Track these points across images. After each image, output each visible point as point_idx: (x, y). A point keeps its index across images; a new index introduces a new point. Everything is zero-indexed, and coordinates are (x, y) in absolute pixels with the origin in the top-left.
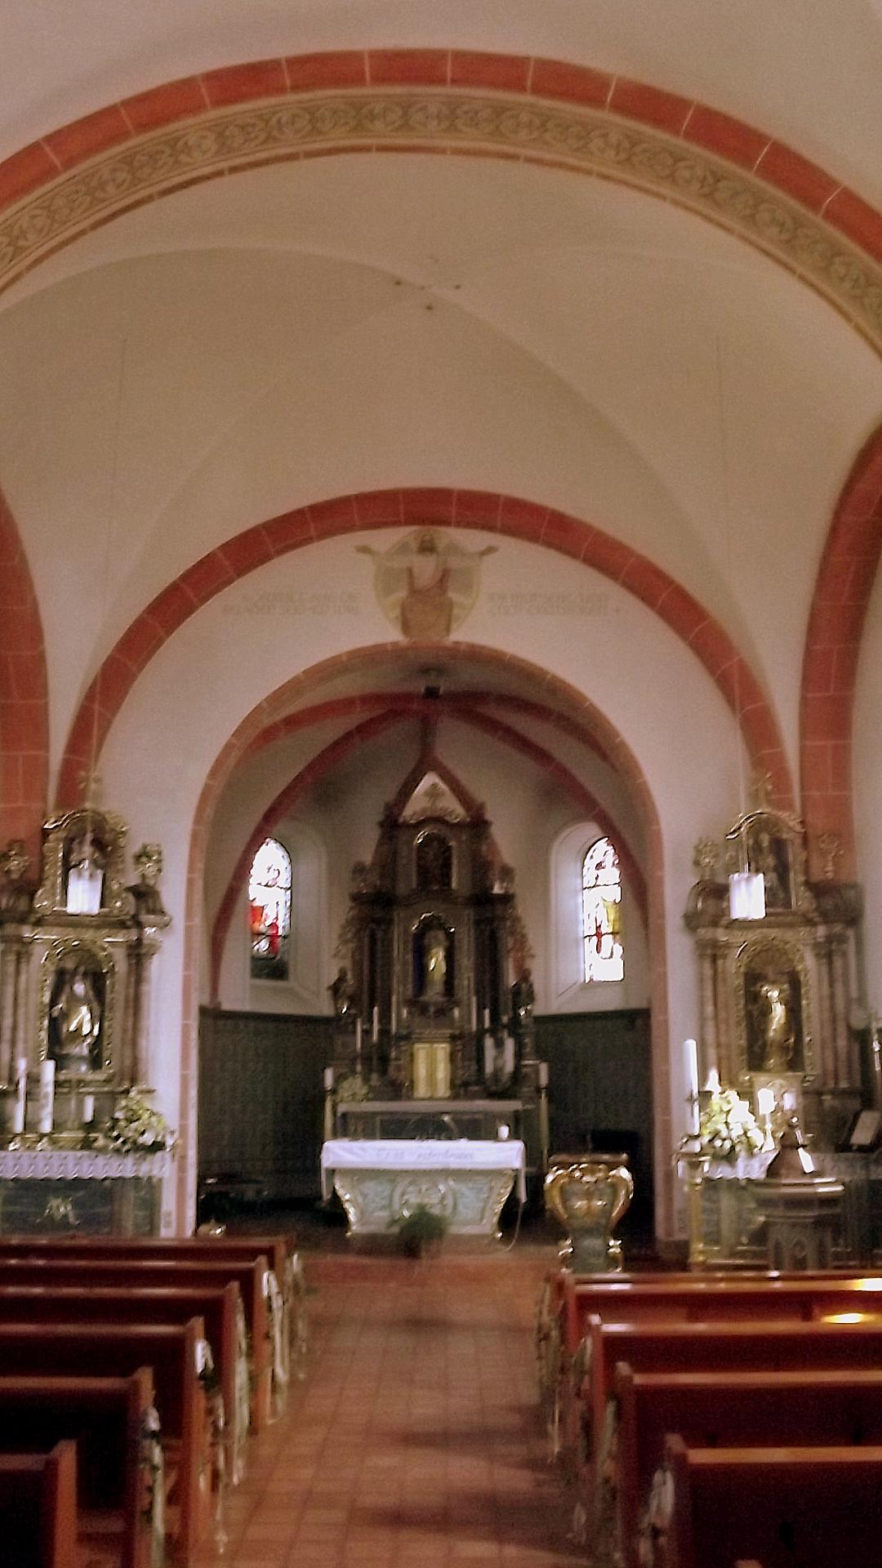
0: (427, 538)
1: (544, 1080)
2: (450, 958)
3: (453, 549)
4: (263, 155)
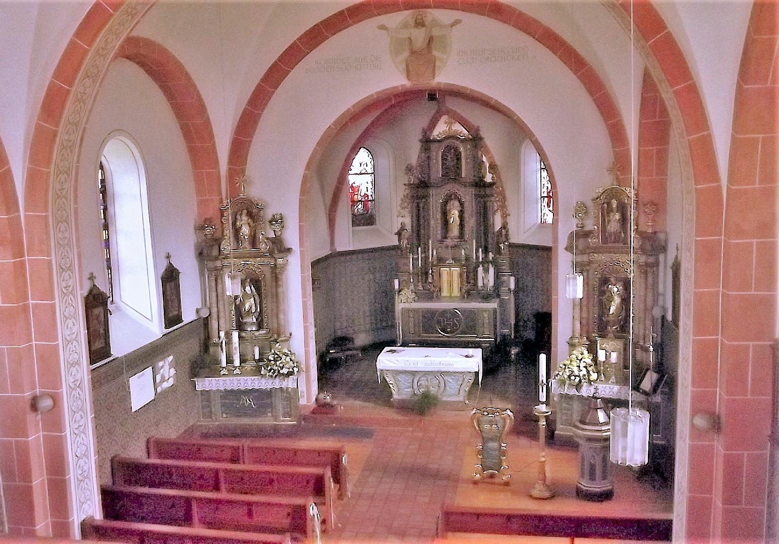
0: (419, 17)
1: (512, 286)
3: (436, 23)
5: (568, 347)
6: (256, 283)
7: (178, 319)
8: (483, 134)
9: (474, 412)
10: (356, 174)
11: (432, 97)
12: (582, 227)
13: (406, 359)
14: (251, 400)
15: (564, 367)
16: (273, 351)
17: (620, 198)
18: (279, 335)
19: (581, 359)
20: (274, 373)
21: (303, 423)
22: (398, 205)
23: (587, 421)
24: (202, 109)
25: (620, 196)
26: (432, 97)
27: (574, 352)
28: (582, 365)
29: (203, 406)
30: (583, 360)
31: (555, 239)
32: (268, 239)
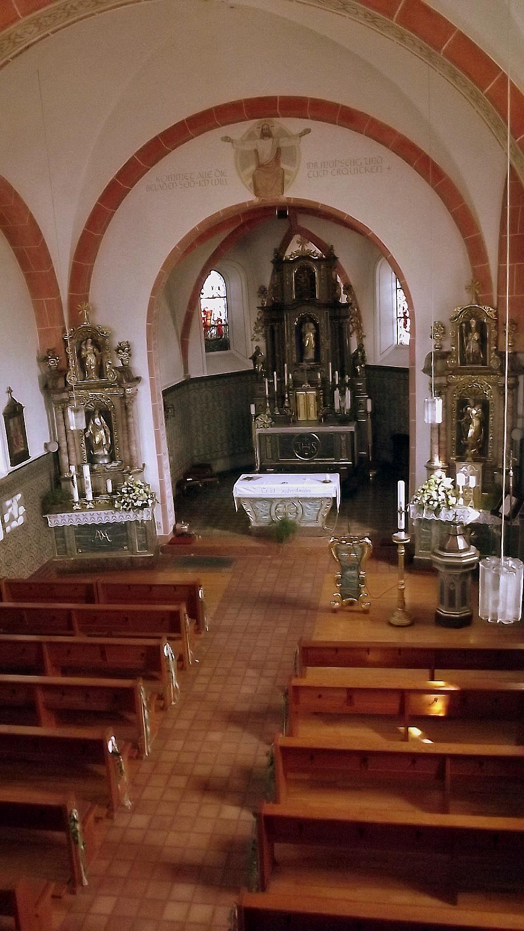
0: (265, 127)
1: (369, 409)
2: (317, 338)
4: (67, 22)
5: (426, 471)
6: (106, 414)
7: (25, 455)
8: (337, 253)
9: (332, 540)
10: (209, 298)
11: (282, 215)
12: (441, 348)
13: (262, 486)
14: (106, 534)
15: (422, 491)
16: (125, 483)
17: (479, 318)
18: (132, 467)
19: (440, 484)
20: (127, 506)
21: (161, 553)
22: (252, 328)
23: (447, 548)
24: (37, 234)
25: (478, 316)
26: (282, 215)
27: (433, 476)
28: (441, 489)
29: (58, 542)
30: (441, 484)
31: (413, 363)
32: (115, 368)
